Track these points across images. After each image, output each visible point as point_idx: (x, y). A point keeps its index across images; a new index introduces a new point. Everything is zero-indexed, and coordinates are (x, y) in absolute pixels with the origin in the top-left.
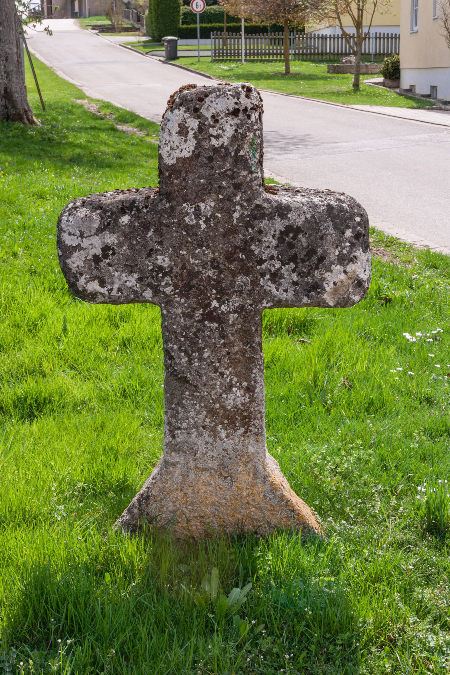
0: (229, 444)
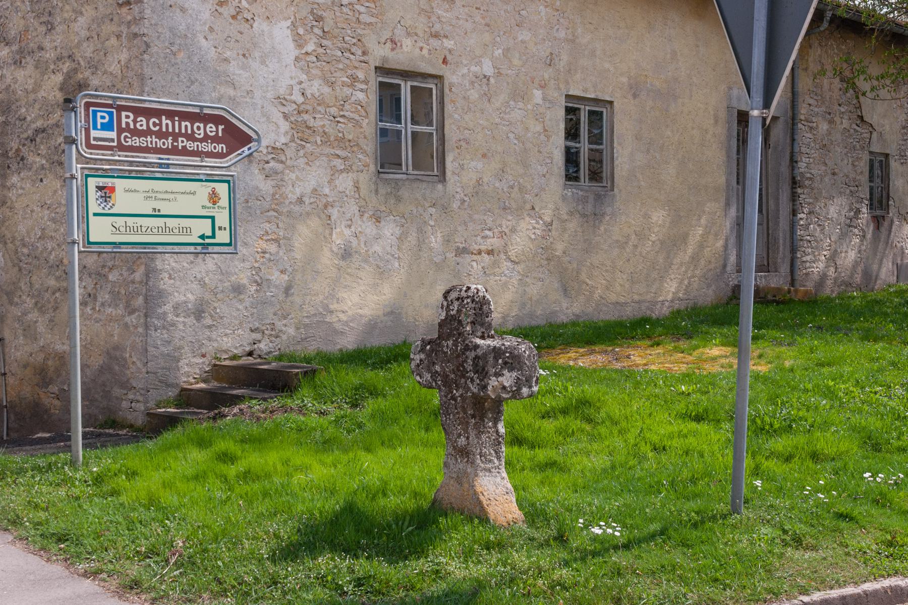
0: (461, 466)
